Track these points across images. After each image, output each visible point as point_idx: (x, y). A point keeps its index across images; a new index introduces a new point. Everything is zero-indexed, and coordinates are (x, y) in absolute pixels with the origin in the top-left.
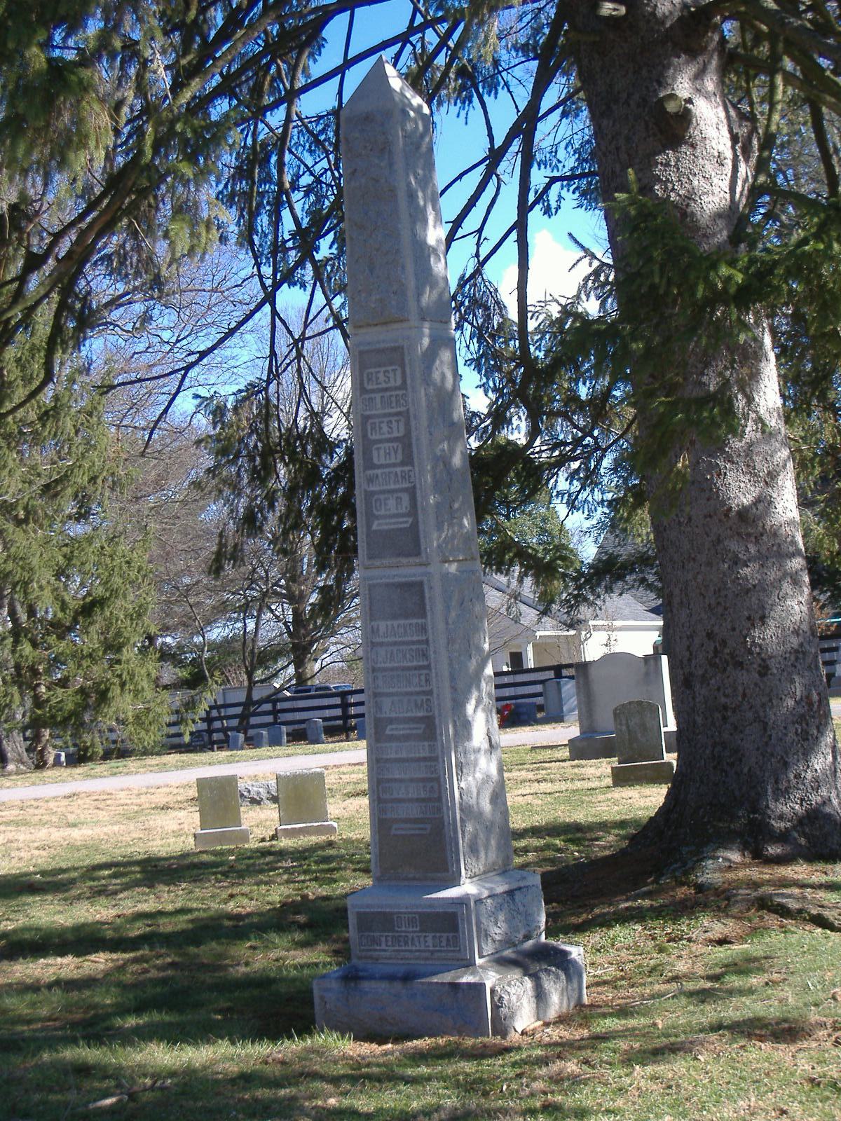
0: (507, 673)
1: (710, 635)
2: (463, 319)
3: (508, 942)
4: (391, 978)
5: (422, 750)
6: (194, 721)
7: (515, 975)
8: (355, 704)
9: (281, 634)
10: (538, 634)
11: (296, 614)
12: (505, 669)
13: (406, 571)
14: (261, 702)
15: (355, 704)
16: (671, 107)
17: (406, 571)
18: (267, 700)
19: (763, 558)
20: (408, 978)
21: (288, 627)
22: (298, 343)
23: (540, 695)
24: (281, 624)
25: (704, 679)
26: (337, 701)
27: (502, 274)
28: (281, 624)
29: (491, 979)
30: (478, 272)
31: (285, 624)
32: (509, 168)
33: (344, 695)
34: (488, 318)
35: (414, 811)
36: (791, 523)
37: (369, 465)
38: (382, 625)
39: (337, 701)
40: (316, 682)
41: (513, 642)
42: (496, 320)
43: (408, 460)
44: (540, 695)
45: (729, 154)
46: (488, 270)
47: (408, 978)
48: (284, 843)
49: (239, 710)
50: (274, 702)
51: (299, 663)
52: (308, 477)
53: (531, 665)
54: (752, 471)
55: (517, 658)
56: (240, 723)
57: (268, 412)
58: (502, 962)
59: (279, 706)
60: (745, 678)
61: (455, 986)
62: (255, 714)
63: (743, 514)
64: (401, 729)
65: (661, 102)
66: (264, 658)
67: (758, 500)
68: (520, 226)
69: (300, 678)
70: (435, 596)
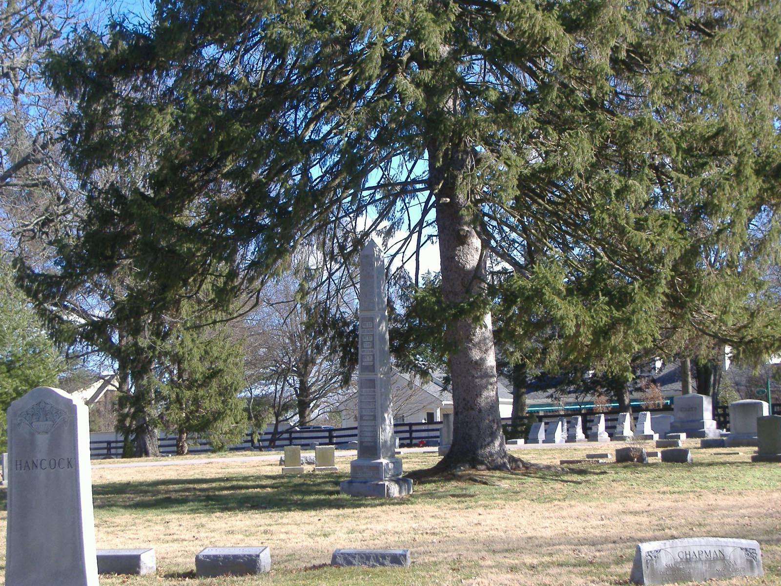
0: (425, 424)
1: (464, 399)
2: (396, 282)
3: (393, 476)
4: (361, 482)
5: (372, 423)
6: (260, 434)
7: (393, 483)
8: (337, 437)
9: (291, 395)
10: (444, 403)
11: (302, 383)
12: (424, 421)
13: (371, 376)
14: (282, 433)
15: (337, 437)
16: (462, 233)
17: (371, 376)
18: (287, 431)
19: (482, 377)
20: (365, 482)
21: (296, 391)
22: (337, 291)
23: (438, 437)
24: (292, 389)
25: (462, 413)
26: (327, 434)
27: (410, 267)
28: (292, 389)
29: (387, 483)
30: (402, 267)
31: (295, 389)
32: (415, 236)
33: (330, 431)
34: (406, 282)
35: (369, 439)
36: (492, 367)
37: (363, 347)
38: (364, 390)
39: (327, 434)
40: (311, 424)
41: (429, 406)
42: (409, 283)
43: (373, 347)
44: (438, 437)
45: (480, 247)
46: (406, 266)
47: (365, 482)
48: (317, 472)
49: (269, 436)
50: (291, 433)
51: (302, 414)
52: (340, 334)
53: (439, 420)
54: (480, 349)
55: (431, 416)
56: (270, 444)
57: (326, 310)
58: (391, 480)
59: (293, 435)
60: (473, 413)
61: (377, 485)
62: (279, 439)
63: (476, 362)
64: (367, 418)
65: (459, 231)
66: (286, 407)
67: (481, 359)
68: (417, 252)
69: (302, 423)
70: (378, 383)
